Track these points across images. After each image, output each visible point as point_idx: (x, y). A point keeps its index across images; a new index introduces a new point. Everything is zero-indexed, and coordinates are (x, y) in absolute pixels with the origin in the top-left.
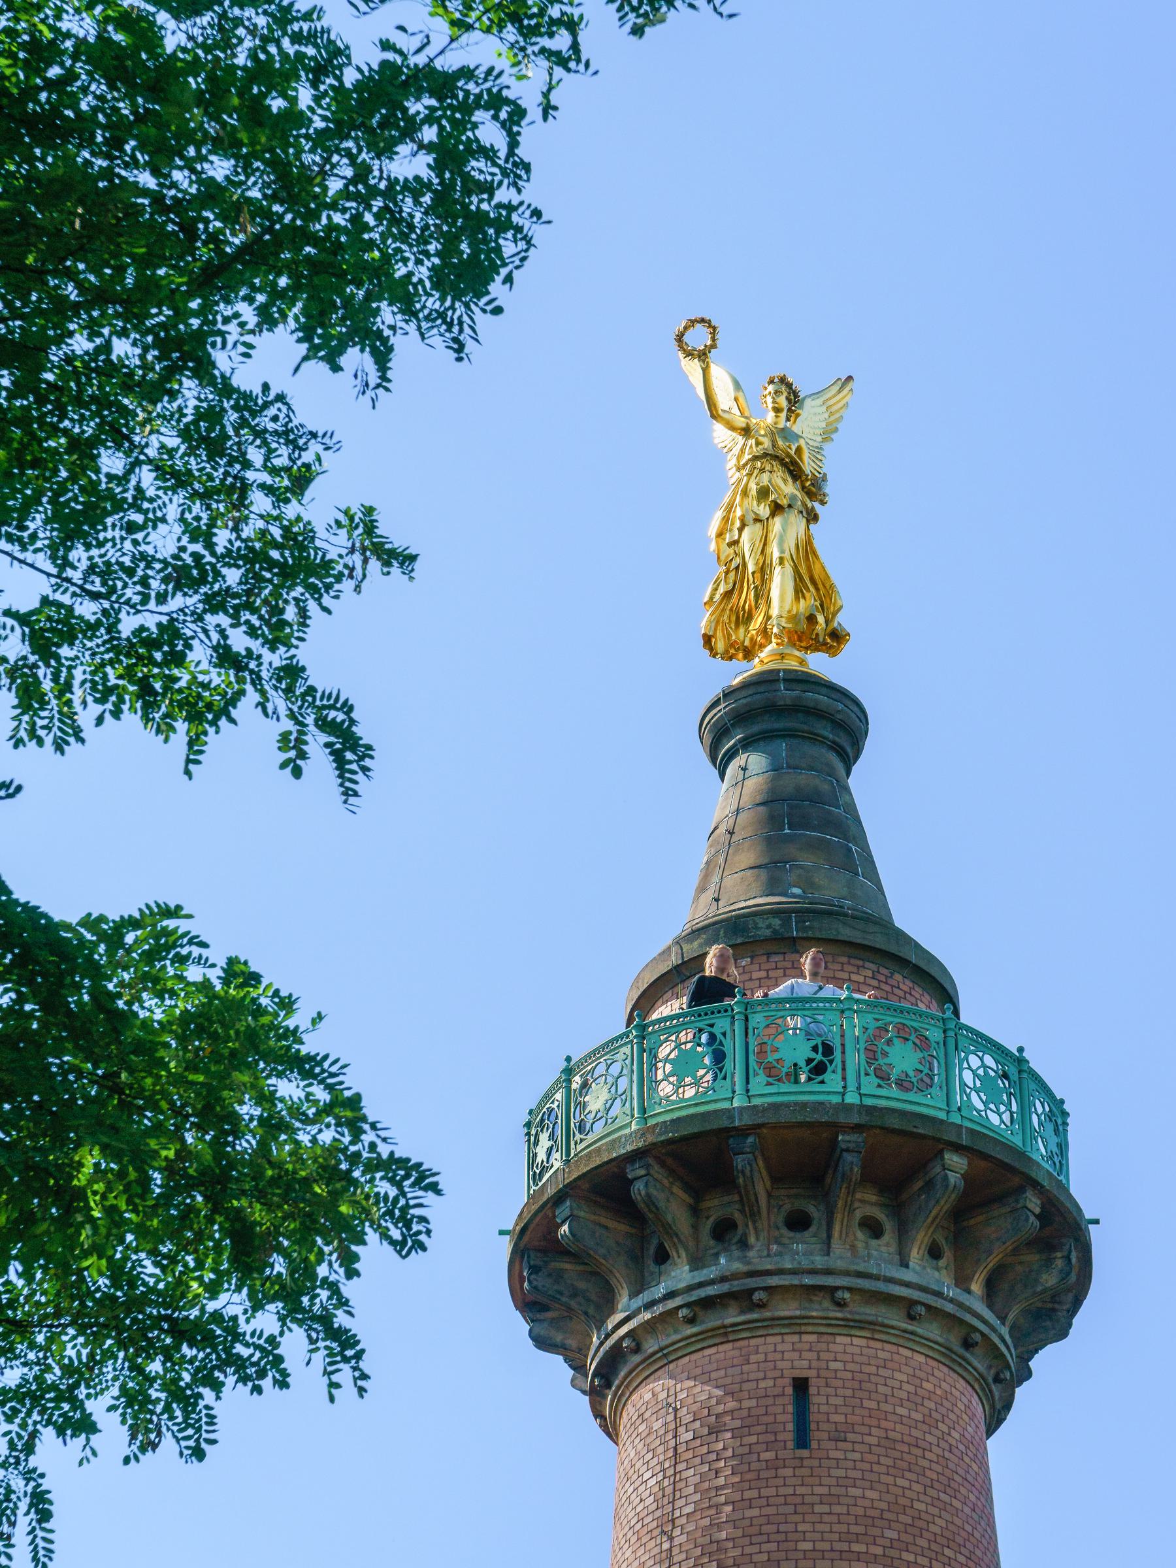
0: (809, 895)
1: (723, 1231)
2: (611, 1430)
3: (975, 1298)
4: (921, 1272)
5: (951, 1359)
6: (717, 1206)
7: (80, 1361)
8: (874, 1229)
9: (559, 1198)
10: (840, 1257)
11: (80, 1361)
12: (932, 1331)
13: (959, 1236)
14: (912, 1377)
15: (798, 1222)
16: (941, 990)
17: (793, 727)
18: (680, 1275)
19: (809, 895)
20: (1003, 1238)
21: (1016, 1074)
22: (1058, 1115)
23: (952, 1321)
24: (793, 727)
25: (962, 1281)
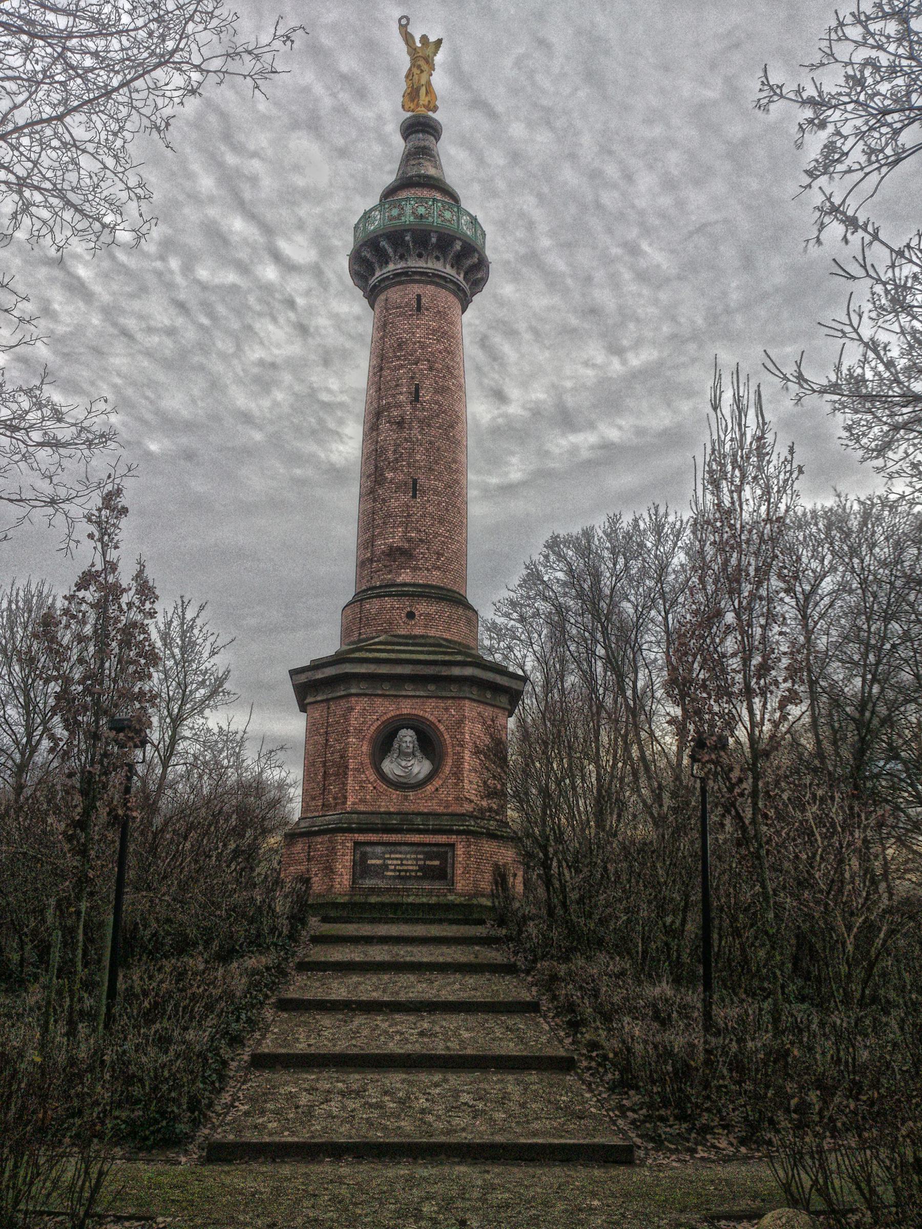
0: (418, 177)
1: (402, 257)
2: (372, 307)
3: (461, 278)
4: (449, 270)
5: (455, 294)
6: (400, 250)
7: (872, 1201)
8: (438, 258)
9: (361, 246)
10: (430, 265)
11: (872, 1201)
12: (450, 285)
13: (457, 262)
14: (446, 299)
15: (420, 256)
16: (455, 198)
17: (420, 129)
18: (391, 267)
19: (418, 177)
20: (466, 264)
21: (474, 221)
22: (484, 234)
23: (455, 283)
24: (420, 129)
25: (458, 274)
